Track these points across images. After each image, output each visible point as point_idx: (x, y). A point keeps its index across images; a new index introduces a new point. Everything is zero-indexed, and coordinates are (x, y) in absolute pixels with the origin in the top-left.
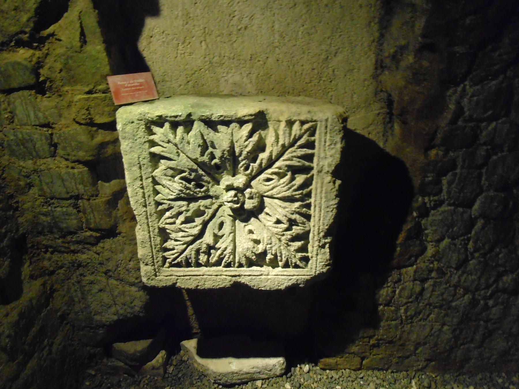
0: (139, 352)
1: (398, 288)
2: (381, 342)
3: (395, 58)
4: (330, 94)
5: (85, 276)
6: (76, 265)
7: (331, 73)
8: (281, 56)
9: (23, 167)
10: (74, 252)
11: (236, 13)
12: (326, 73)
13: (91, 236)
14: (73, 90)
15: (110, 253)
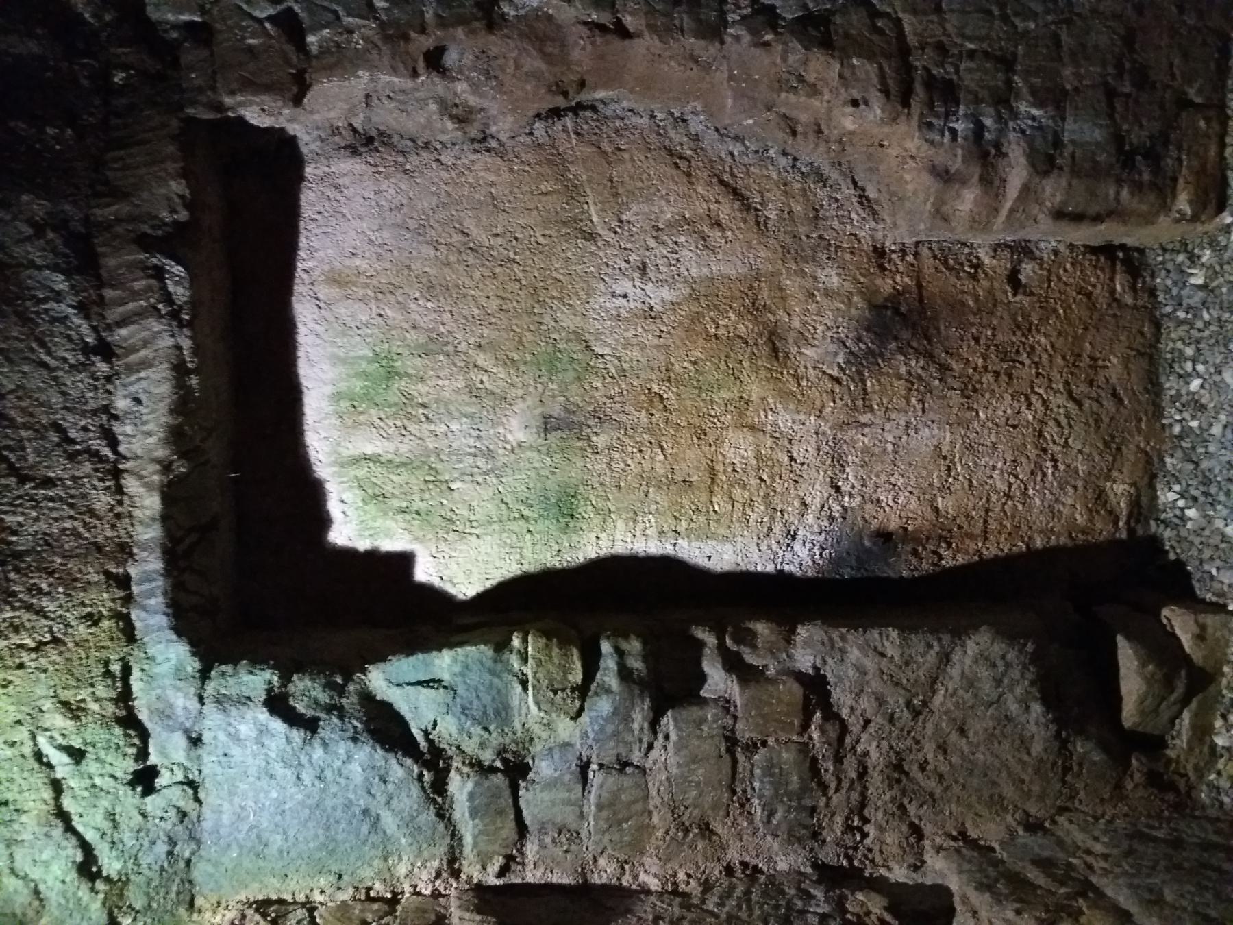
0: (1143, 665)
1: (962, 45)
2: (1127, 65)
3: (463, 118)
4: (541, 240)
5: (926, 761)
6: (896, 775)
7: (499, 240)
8: (472, 341)
9: (667, 833)
10: (863, 773)
11: (399, 423)
12: (501, 249)
13: (823, 731)
14: (520, 715)
15: (864, 698)
